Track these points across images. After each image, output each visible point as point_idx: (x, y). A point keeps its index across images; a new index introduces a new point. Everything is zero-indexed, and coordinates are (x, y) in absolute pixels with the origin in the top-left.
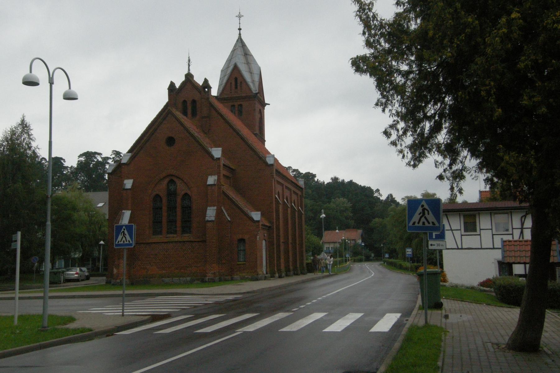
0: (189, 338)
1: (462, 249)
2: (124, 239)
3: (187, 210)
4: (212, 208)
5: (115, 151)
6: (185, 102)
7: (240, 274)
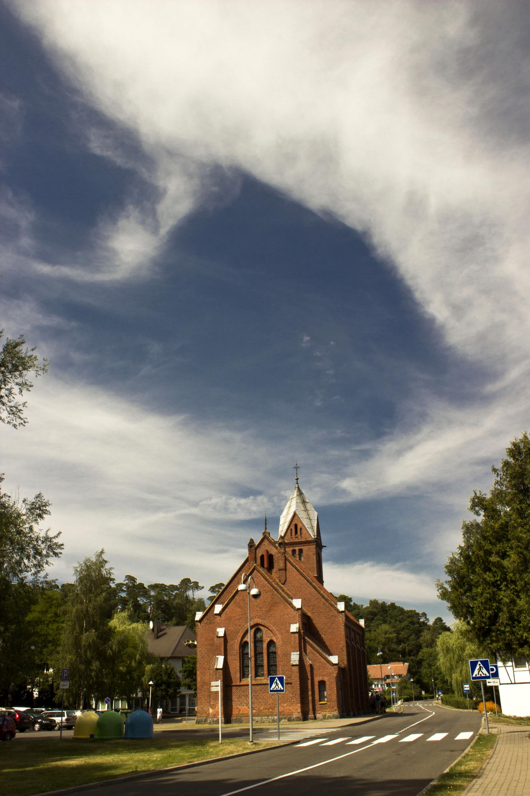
0: (341, 748)
1: (515, 683)
2: (277, 687)
3: (272, 655)
4: (295, 653)
5: (130, 576)
6: (262, 557)
7: (322, 713)
